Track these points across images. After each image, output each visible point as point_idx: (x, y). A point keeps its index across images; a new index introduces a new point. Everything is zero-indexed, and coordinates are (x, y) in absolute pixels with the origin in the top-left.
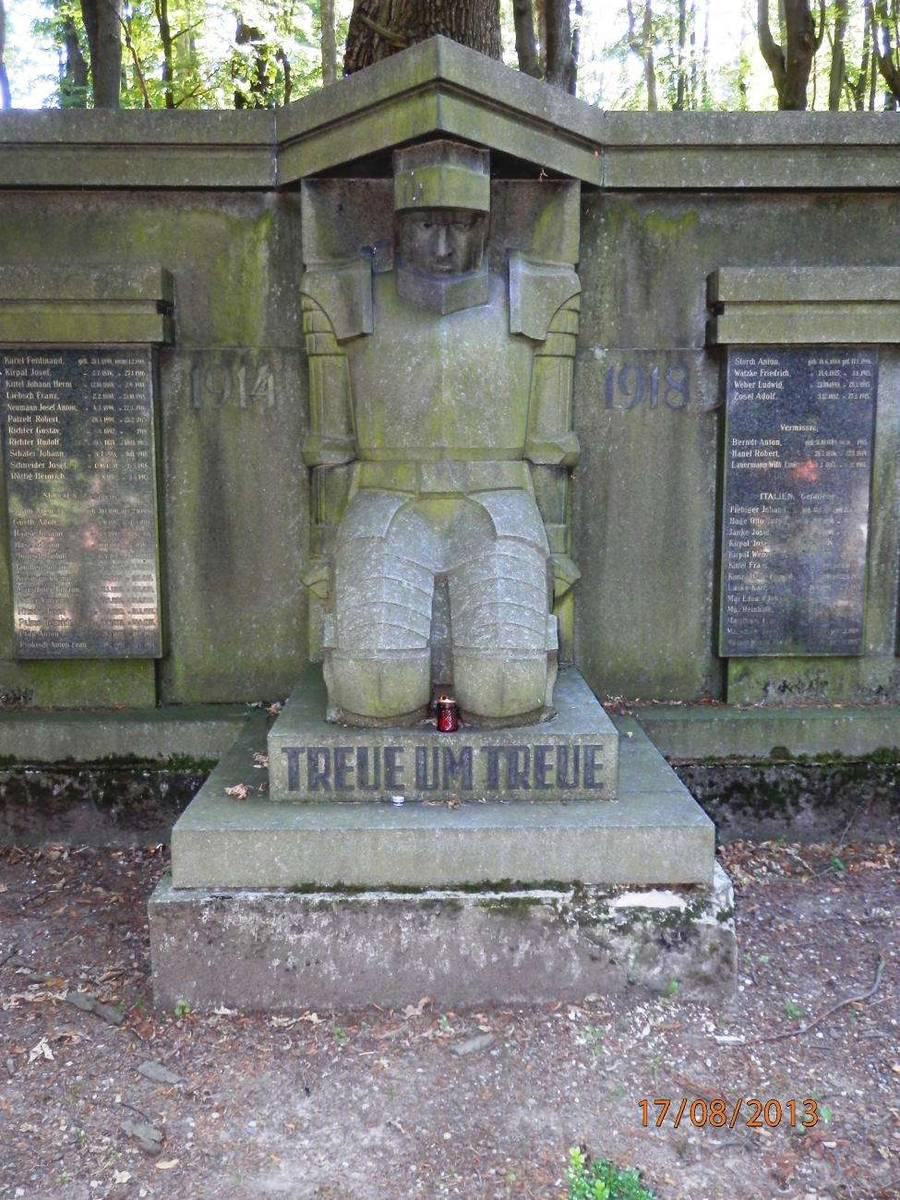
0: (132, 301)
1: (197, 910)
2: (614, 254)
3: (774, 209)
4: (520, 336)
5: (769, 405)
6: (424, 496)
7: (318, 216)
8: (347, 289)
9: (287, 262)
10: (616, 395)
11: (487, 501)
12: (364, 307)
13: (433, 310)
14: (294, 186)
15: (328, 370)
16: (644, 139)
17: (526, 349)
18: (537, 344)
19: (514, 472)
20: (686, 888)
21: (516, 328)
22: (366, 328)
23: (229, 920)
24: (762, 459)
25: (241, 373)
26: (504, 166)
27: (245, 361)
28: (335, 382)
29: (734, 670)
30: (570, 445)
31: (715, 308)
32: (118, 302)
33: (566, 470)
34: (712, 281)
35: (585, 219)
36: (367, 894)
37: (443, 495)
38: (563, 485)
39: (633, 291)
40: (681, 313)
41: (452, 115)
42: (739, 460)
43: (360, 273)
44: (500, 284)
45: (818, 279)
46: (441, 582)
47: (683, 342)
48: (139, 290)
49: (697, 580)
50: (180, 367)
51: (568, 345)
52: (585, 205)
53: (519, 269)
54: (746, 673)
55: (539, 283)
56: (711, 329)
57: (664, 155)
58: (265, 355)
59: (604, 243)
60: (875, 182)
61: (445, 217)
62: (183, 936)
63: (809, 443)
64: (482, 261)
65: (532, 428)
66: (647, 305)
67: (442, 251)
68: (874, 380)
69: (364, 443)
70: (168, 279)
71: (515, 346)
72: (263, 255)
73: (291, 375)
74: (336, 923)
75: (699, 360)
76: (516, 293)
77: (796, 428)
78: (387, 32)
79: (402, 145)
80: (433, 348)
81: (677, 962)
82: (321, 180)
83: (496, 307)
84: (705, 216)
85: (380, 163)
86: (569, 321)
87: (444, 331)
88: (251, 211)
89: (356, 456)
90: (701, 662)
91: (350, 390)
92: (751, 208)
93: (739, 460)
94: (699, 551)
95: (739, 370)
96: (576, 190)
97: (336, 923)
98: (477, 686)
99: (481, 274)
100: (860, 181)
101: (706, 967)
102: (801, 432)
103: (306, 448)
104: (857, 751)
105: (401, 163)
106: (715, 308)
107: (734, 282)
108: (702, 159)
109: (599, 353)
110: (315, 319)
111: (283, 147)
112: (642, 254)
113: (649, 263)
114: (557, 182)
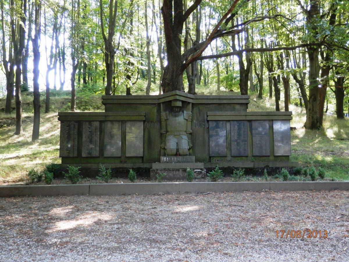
0: (142, 116)
1: (155, 170)
2: (196, 110)
3: (214, 105)
4: (185, 119)
5: (214, 127)
6: (175, 135)
7: (163, 107)
8: (166, 114)
9: (159, 111)
10: (197, 126)
11: (182, 136)
12: (168, 116)
13: (176, 116)
14: (160, 103)
15: (163, 123)
16: (199, 98)
17: (186, 121)
18: (187, 120)
19: (185, 133)
20: (201, 169)
21: (185, 118)
22: (168, 118)
23: (158, 171)
25: (153, 124)
26: (183, 102)
27: (153, 122)
28: (164, 124)
29: (212, 158)
30: (191, 131)
31: (207, 116)
32: (140, 116)
33: (191, 134)
34: (207, 113)
35: (192, 106)
36: (201, 28)
37: (177, 135)
38: (190, 135)
39: (198, 114)
40: (204, 117)
41: (178, 97)
43: (168, 112)
44: (183, 113)
45: (219, 113)
46: (177, 143)
47: (204, 120)
48: (143, 114)
49: (207, 148)
50: (146, 123)
51: (191, 120)
52: (192, 105)
53: (185, 112)
54: (213, 159)
55: (187, 113)
56: (207, 119)
57: (201, 100)
58: (156, 122)
59: (195, 109)
60: (224, 102)
61: (178, 107)
62: (153, 173)
64: (181, 111)
65: (187, 129)
66: (200, 115)
67: (177, 110)
68: (226, 124)
69: (168, 130)
70: (145, 113)
71: (185, 120)
72: (156, 110)
73: (159, 124)
74: (168, 172)
75: (206, 122)
76: (185, 114)
78: (168, 81)
79: (173, 100)
80: (176, 120)
81: (200, 176)
82: (163, 103)
83: (182, 116)
84: (206, 106)
85: (170, 101)
86: (191, 118)
87: (177, 118)
88: (154, 106)
89: (167, 132)
90: (208, 157)
91: (166, 125)
92: (211, 105)
94: (207, 145)
95: (210, 123)
96: (191, 104)
97: (168, 172)
98: (181, 152)
99: (181, 112)
100: (223, 102)
101: (203, 176)
103: (161, 132)
104: (226, 167)
105: (173, 102)
106: (207, 116)
107: (209, 113)
108: (205, 100)
109: (194, 121)
110: (162, 117)
111: (158, 99)
112: (199, 110)
113: (200, 111)
114: (189, 103)
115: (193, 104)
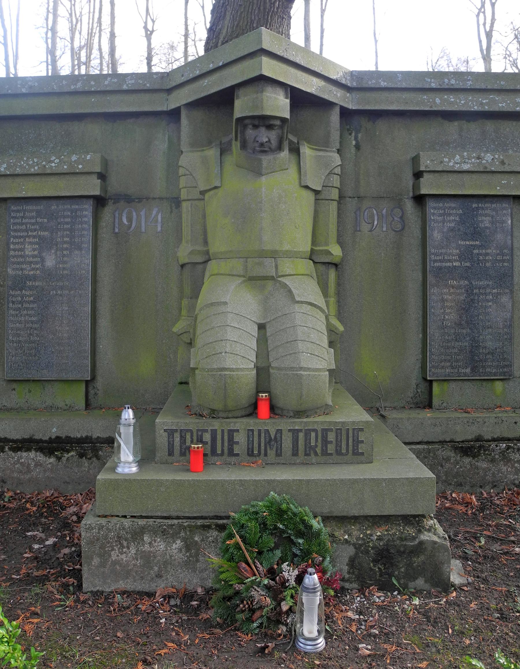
24: (449, 261)
31: (418, 175)
42: (435, 261)
46: (261, 327)
56: (416, 186)
63: (476, 251)
77: (468, 243)
86: (336, 181)
93: (435, 261)
96: (337, 110)
102: (472, 245)
115: (345, 113)
